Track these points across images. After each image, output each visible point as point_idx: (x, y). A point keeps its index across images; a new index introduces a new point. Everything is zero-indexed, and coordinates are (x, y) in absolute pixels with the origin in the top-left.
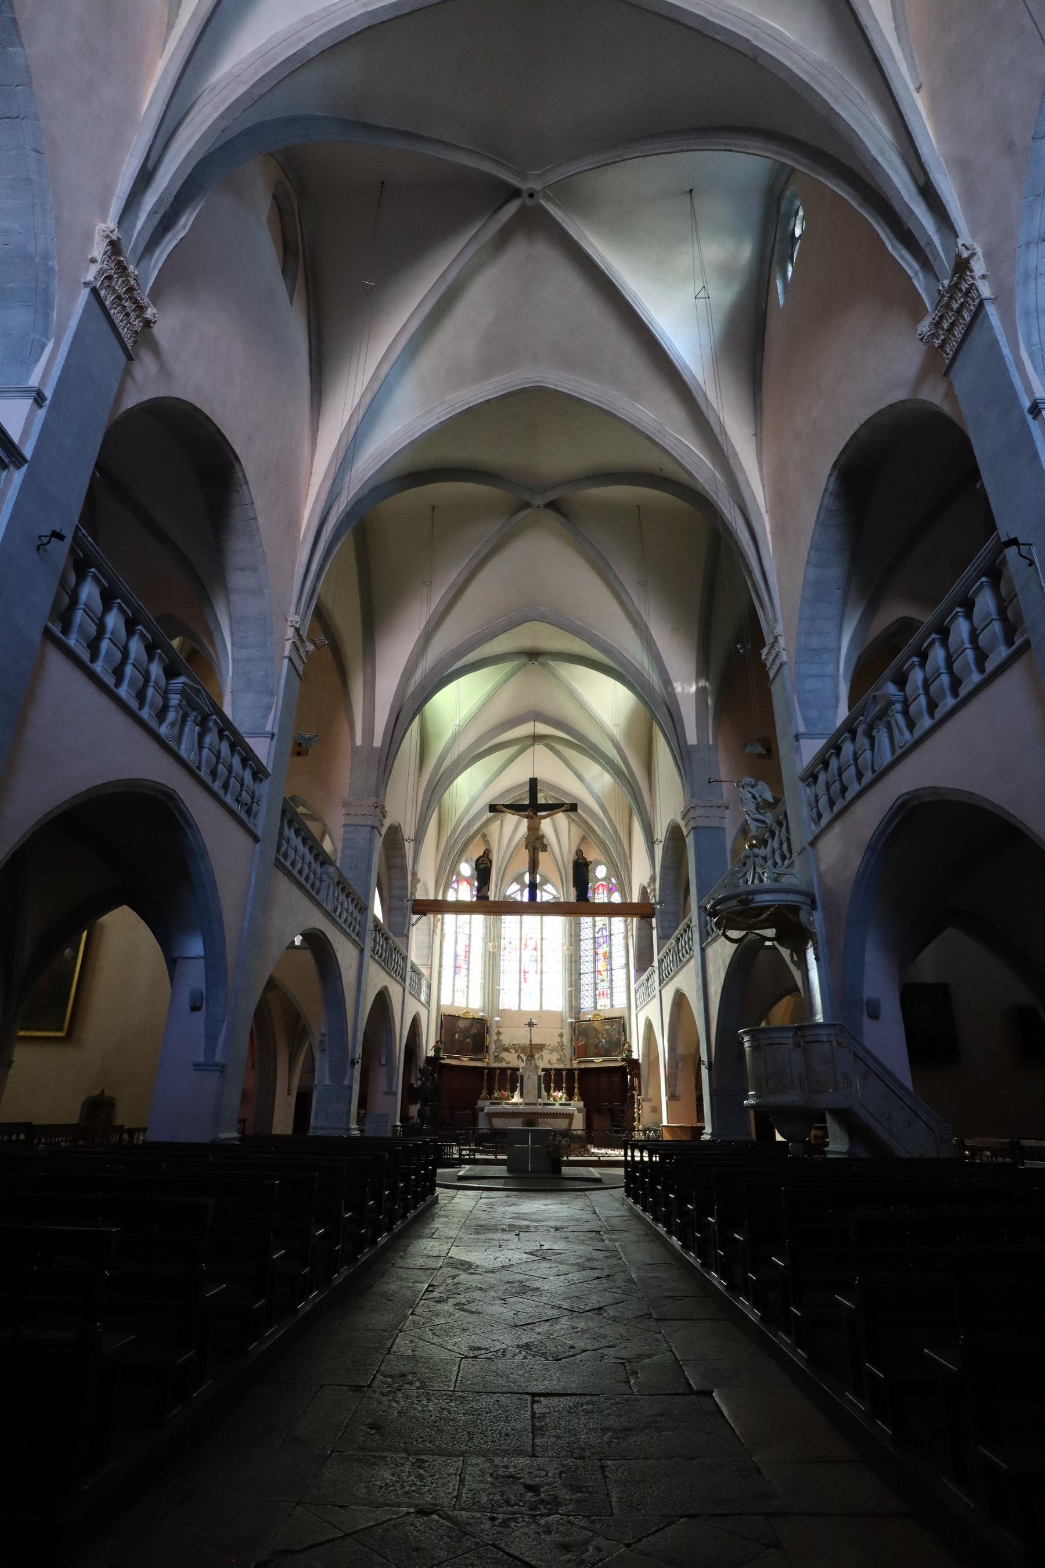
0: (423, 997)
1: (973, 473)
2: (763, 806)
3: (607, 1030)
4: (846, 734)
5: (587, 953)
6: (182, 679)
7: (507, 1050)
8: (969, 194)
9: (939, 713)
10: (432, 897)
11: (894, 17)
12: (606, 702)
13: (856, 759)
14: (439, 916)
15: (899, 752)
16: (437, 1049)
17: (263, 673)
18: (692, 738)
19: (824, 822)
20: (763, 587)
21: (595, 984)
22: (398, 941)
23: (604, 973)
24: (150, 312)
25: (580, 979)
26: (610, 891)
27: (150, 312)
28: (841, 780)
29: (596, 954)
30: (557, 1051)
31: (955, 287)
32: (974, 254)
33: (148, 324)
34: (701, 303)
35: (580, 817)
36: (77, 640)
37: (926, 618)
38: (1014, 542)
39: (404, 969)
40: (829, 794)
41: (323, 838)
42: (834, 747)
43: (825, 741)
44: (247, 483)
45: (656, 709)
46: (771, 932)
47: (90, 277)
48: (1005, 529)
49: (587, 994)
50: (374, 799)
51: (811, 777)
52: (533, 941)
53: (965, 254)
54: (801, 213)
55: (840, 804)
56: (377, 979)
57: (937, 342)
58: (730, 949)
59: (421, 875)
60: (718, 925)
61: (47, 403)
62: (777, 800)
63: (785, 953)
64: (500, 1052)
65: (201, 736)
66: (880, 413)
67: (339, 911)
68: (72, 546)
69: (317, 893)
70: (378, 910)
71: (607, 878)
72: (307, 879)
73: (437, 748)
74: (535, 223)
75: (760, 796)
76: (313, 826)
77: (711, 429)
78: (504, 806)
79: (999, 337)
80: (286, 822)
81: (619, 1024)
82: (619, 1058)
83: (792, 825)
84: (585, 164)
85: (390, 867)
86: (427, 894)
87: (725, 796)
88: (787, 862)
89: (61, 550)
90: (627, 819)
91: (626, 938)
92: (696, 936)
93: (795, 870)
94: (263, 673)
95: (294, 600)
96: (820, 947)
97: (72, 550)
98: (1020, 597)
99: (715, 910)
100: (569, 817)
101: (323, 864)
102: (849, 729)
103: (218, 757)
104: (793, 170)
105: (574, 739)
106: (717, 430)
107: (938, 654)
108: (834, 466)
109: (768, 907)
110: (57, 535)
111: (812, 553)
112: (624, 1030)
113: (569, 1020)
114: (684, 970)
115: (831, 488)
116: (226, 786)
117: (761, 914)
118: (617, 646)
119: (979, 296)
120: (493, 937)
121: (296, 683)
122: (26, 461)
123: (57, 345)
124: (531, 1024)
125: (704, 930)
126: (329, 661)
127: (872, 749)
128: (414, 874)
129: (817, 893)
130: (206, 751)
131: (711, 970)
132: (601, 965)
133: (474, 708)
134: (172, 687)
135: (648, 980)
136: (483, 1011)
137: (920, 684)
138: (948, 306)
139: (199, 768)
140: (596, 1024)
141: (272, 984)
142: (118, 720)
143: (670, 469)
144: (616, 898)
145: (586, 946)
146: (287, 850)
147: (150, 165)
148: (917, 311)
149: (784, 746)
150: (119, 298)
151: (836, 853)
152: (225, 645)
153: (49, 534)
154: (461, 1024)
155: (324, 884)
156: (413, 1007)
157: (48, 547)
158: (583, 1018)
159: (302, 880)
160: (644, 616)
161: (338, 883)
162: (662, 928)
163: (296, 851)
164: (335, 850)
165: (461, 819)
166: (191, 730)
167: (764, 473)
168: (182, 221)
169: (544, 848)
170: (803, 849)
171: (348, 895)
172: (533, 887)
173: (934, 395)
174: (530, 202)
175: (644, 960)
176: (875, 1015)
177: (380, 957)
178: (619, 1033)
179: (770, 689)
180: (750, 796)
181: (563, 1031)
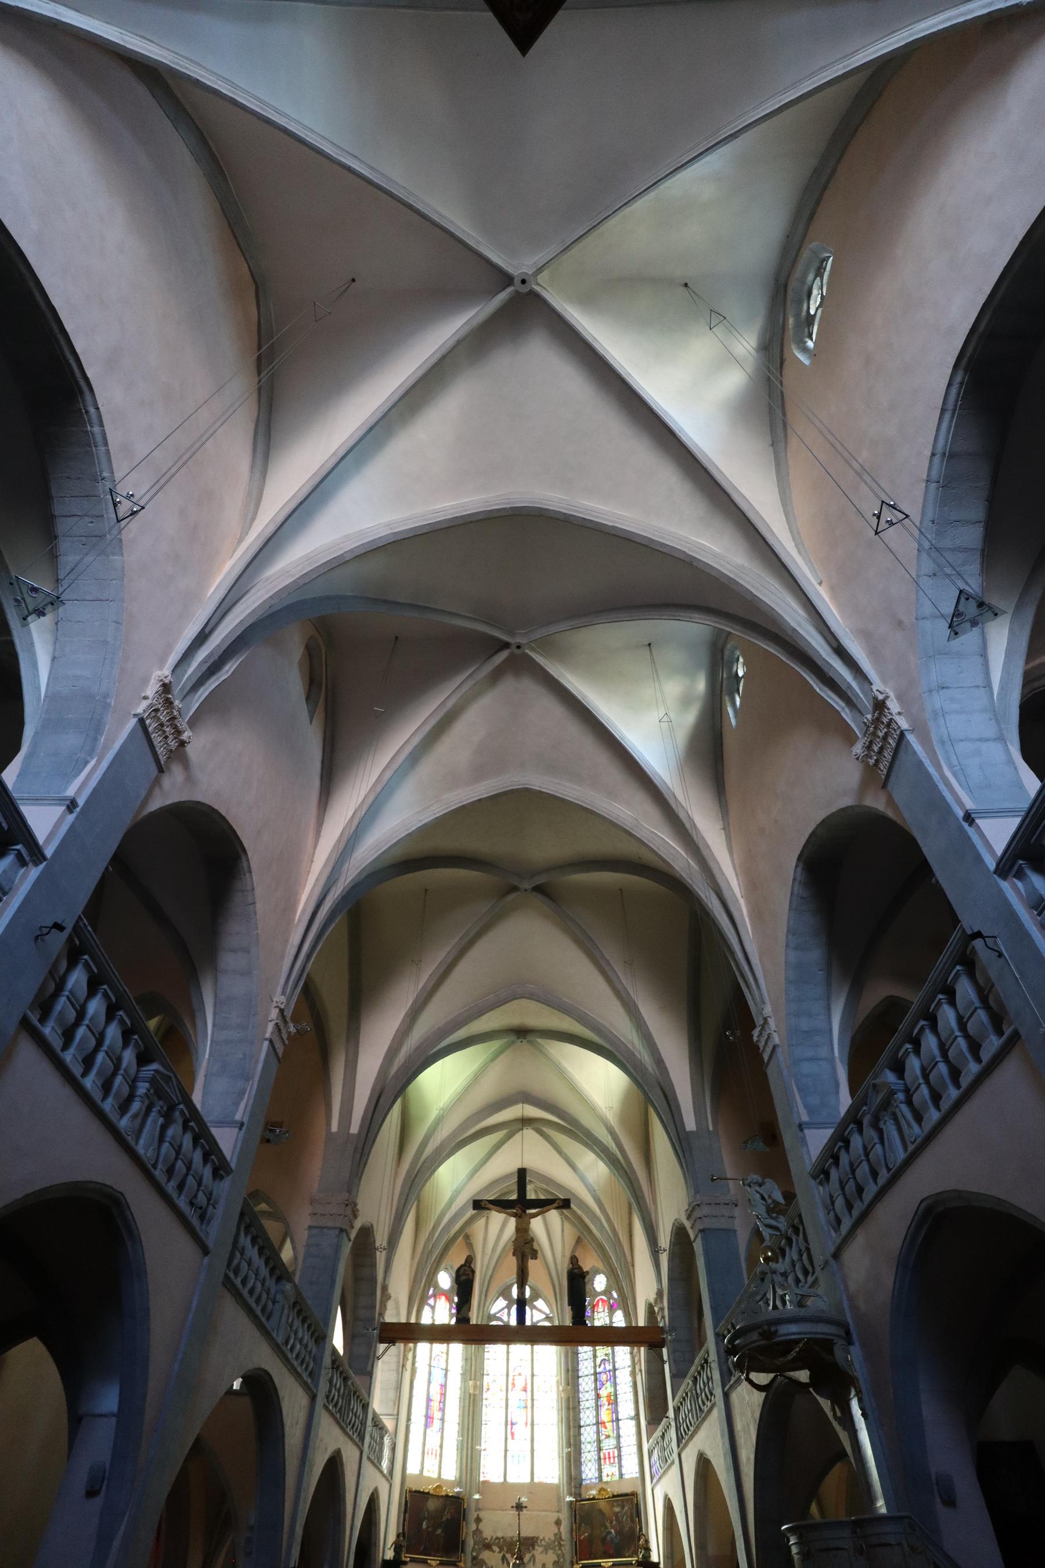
0: (385, 1465)
1: (924, 868)
2: (774, 1209)
3: (616, 1514)
4: (852, 1126)
5: (587, 1396)
6: (155, 1066)
7: (488, 1546)
8: (874, 653)
9: (945, 1105)
10: (403, 1320)
11: (794, 539)
12: (599, 1083)
13: (867, 1155)
14: (411, 1345)
15: (911, 1148)
16: (398, 1548)
17: (241, 1056)
18: (690, 1124)
19: (845, 1228)
20: (746, 968)
21: (599, 1441)
22: (357, 1380)
23: (609, 1425)
24: (185, 736)
25: (580, 1434)
26: (612, 1309)
27: (185, 736)
28: (855, 1178)
29: (598, 1396)
30: (553, 1549)
31: (877, 721)
32: (887, 697)
33: (182, 744)
34: (665, 725)
35: (574, 1213)
36: (53, 1028)
37: (914, 998)
38: (978, 935)
39: (364, 1424)
40: (844, 1194)
41: (282, 1243)
42: (841, 1139)
43: (832, 1131)
44: (250, 872)
45: (650, 1090)
46: (803, 1376)
47: (140, 710)
48: (969, 922)
49: (589, 1456)
50: (346, 1195)
51: (821, 1174)
52: (522, 1378)
53: (881, 697)
54: (741, 660)
55: (858, 1209)
56: (330, 1438)
57: (872, 762)
58: (759, 1397)
59: (391, 1290)
60: (739, 1366)
61: (78, 809)
62: (790, 1196)
63: (825, 1404)
64: (479, 1552)
65: (164, 1128)
66: (833, 814)
67: (291, 1341)
68: (70, 935)
69: (268, 1318)
70: (338, 1340)
71: (607, 1292)
72: (258, 1301)
73: (418, 1135)
74: (521, 665)
75: (770, 1197)
76: (272, 1228)
77: (683, 825)
78: (491, 1202)
79: (923, 760)
80: (242, 1228)
81: (631, 1503)
82: (634, 1560)
83: (810, 1232)
84: (562, 627)
85: (357, 1279)
86: (398, 1314)
87: (733, 1191)
88: (810, 1279)
89: (57, 941)
90: (626, 1216)
91: (633, 1374)
92: (716, 1376)
93: (820, 1290)
94: (241, 1056)
95: (282, 981)
96: (866, 1398)
97: (70, 939)
98: (997, 986)
99: (734, 1346)
100: (562, 1214)
101: (279, 1279)
102: (854, 1118)
103: (178, 1152)
104: (729, 633)
105: (565, 1123)
106: (688, 825)
107: (930, 1042)
108: (799, 859)
109: (797, 1342)
110: (59, 927)
111: (790, 937)
112: (638, 1515)
113: (569, 1499)
114: (706, 1424)
115: (799, 878)
116: (181, 1187)
117: (789, 1352)
118: (607, 1025)
119: (899, 727)
120: (474, 1372)
121: (274, 1064)
122: (45, 858)
123: (99, 762)
124: (519, 1507)
125: (725, 1367)
126: (314, 1036)
127: (882, 1142)
128: (385, 1288)
129: (850, 1321)
130: (166, 1145)
131: (739, 1425)
132: (605, 1415)
133: (459, 1089)
134: (142, 1074)
135: (663, 1436)
136: (459, 1483)
137: (918, 1072)
138: (874, 734)
139: (155, 1166)
140: (603, 1505)
141: (198, 1446)
142: (79, 1113)
143: (648, 857)
144: (619, 1320)
145: (586, 1384)
146: (239, 1265)
147: (207, 630)
148: (850, 738)
149: (788, 1137)
150: (162, 725)
151: (865, 1269)
152: (206, 1024)
153: (51, 925)
154: (432, 1505)
155: (278, 1306)
156: (372, 1480)
157: (47, 937)
158: (585, 1496)
159: (251, 1301)
160: (631, 993)
161: (295, 1304)
162: (675, 1361)
163: (249, 1263)
164: (296, 1258)
165: (442, 1214)
166: (154, 1122)
167: (735, 856)
168: (227, 668)
169: (534, 1255)
170: (826, 1263)
171: (303, 1321)
172: (522, 1304)
173: (877, 802)
174: (517, 652)
175: (655, 1408)
176: (950, 1502)
177: (335, 1406)
178: (633, 1521)
179: (765, 1074)
180: (758, 1195)
181: (561, 1516)
